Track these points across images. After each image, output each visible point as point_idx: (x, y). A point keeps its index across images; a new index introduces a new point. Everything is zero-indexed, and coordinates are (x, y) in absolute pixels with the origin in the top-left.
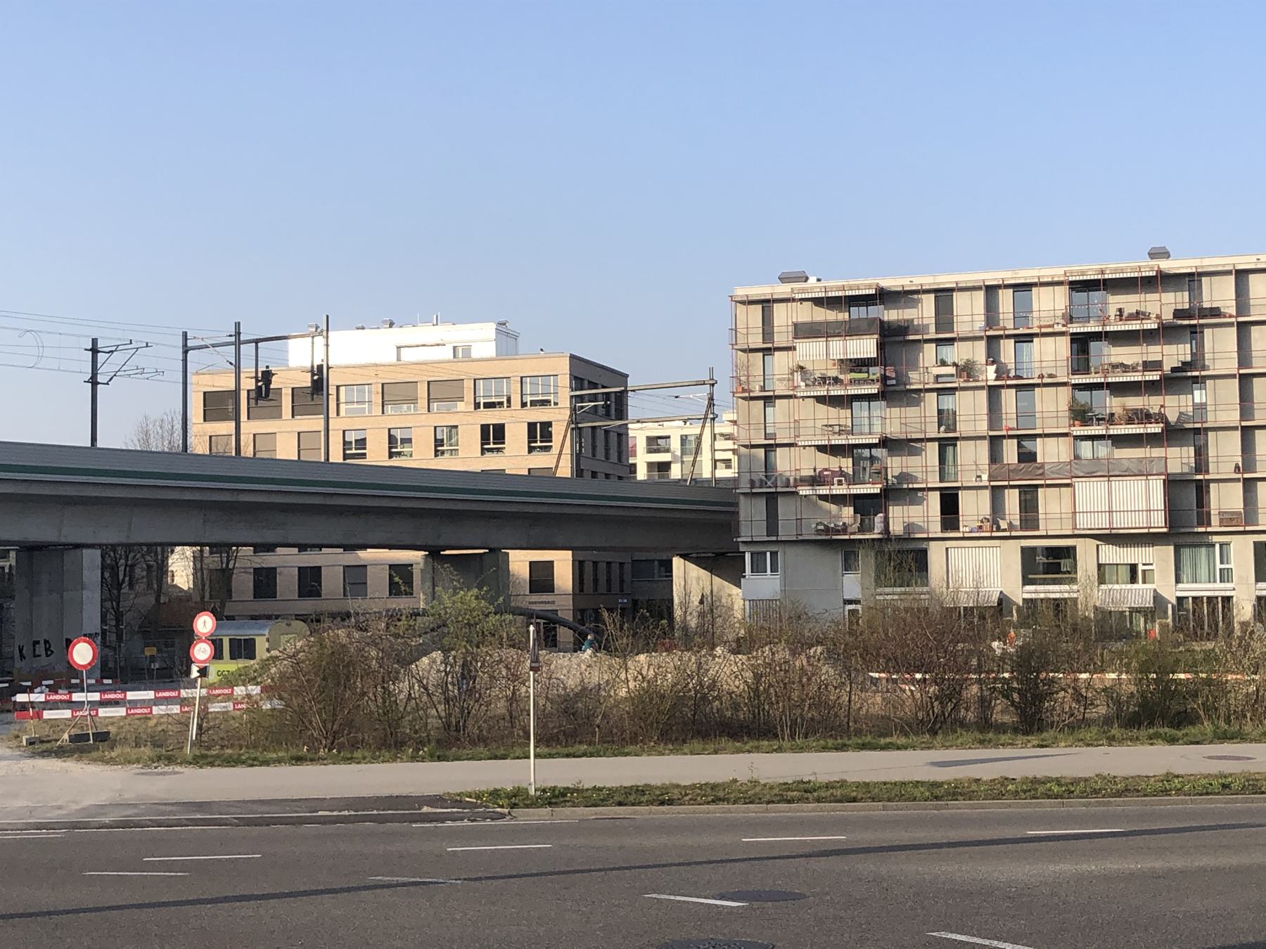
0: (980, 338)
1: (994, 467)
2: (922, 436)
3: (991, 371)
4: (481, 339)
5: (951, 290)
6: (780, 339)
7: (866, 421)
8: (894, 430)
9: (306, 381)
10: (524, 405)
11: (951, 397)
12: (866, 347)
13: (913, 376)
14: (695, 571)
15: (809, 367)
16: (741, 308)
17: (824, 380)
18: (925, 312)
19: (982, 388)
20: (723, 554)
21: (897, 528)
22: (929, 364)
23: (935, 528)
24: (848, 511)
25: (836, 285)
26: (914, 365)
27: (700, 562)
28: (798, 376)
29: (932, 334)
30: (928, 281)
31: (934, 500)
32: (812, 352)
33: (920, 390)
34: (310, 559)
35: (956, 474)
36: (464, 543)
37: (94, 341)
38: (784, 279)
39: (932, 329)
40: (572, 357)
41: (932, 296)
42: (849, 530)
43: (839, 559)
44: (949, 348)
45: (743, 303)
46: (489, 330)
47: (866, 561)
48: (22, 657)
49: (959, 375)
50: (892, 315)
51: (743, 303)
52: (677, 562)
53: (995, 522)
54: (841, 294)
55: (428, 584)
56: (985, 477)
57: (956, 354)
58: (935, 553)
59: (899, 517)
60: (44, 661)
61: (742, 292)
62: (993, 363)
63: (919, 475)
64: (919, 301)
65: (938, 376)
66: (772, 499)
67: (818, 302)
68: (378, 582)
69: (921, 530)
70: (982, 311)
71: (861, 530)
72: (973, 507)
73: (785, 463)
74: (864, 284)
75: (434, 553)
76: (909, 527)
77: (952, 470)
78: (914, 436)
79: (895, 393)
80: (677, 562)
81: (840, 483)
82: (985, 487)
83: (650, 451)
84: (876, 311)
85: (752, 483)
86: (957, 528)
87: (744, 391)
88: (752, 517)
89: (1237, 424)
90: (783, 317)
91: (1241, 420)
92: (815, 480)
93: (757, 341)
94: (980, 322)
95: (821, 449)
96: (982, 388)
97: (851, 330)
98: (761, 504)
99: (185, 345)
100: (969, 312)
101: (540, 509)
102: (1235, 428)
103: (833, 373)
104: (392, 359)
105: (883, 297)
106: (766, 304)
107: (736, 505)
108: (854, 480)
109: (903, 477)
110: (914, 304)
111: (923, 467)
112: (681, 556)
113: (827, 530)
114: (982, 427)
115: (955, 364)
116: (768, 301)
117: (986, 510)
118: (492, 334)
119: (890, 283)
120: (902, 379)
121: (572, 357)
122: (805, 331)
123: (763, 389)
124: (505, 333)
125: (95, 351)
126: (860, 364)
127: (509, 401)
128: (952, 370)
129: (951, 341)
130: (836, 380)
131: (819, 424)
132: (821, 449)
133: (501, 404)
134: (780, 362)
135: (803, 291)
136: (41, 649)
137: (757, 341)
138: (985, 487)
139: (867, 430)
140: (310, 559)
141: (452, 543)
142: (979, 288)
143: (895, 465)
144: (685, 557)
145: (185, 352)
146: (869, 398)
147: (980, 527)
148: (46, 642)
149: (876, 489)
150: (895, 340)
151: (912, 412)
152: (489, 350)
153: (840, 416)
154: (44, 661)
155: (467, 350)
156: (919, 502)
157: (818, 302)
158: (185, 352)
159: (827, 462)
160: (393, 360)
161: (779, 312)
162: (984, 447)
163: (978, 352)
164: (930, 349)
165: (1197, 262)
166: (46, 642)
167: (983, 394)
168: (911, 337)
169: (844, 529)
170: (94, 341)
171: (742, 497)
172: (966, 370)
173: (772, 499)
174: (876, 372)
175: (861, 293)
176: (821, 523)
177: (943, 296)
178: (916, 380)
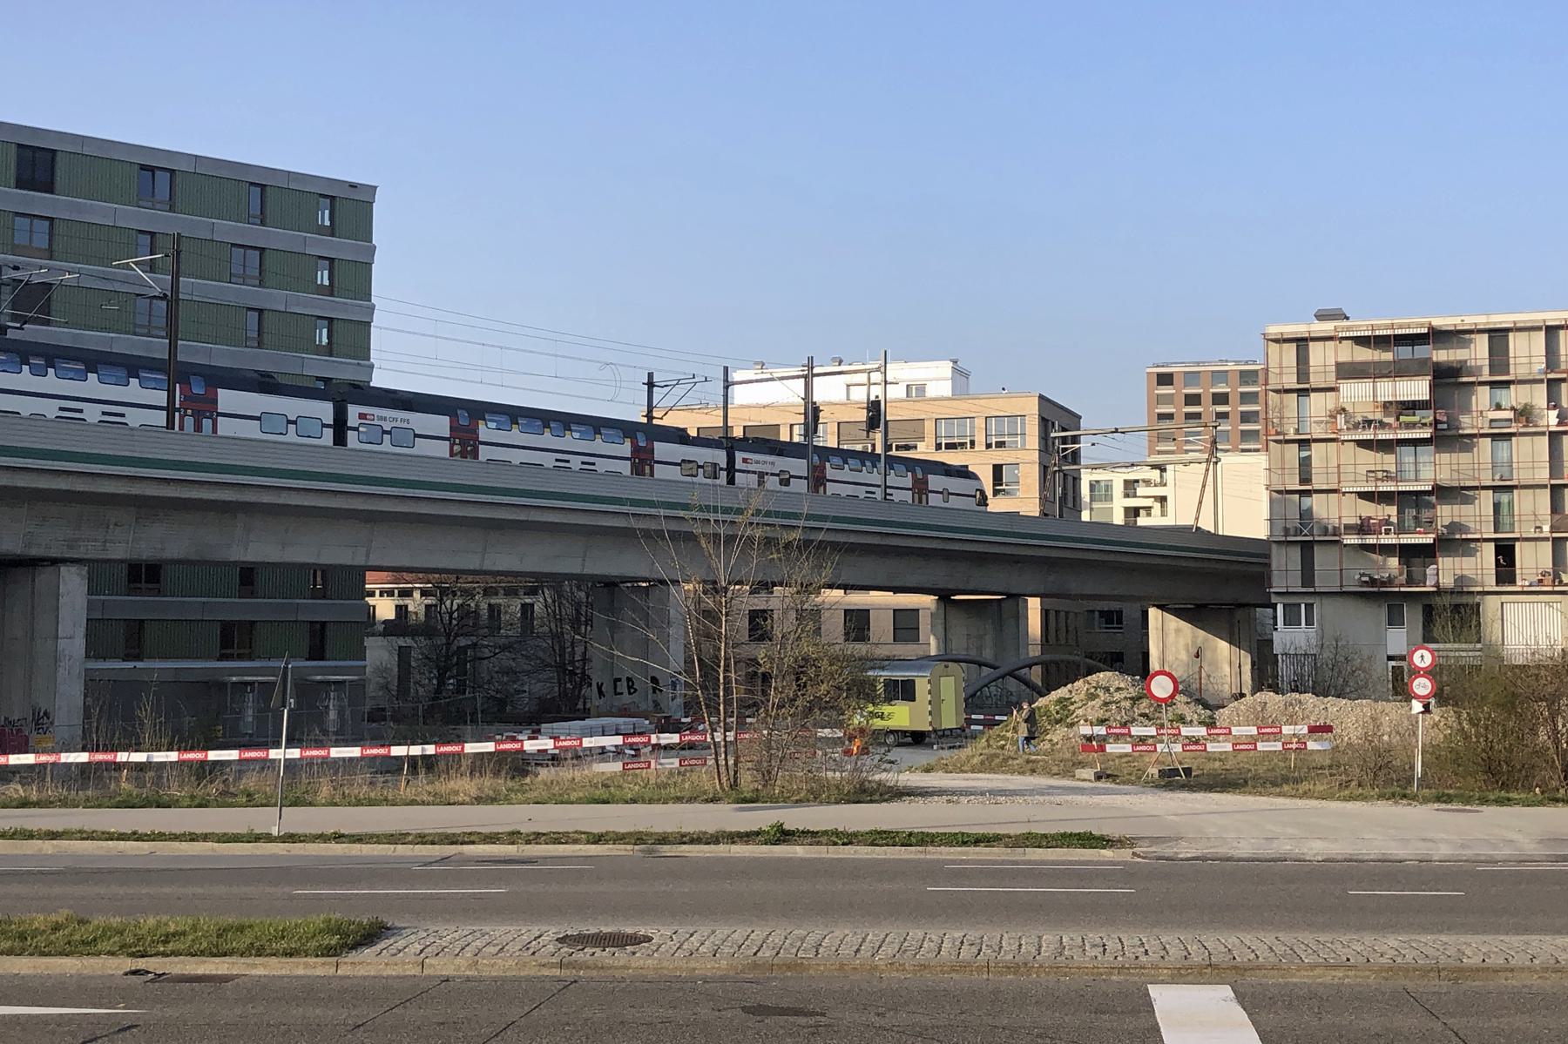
0: (1541, 381)
1: (1557, 517)
2: (1476, 483)
3: (1553, 416)
4: (937, 378)
5: (1507, 330)
6: (1315, 380)
7: (1412, 468)
8: (1445, 477)
9: (862, 416)
10: (989, 446)
11: (1505, 444)
12: (1418, 388)
13: (1465, 420)
14: (1173, 622)
15: (1349, 409)
16: (1274, 347)
17: (1368, 423)
18: (1478, 352)
19: (1543, 434)
20: (1205, 606)
21: (1447, 581)
22: (1481, 409)
23: (1490, 583)
24: (1394, 562)
25: (1383, 324)
26: (1467, 409)
27: (1179, 613)
28: (1341, 419)
29: (1486, 377)
30: (1482, 320)
31: (1489, 549)
32: (1357, 394)
33: (1474, 436)
34: (858, 599)
35: (1512, 525)
36: (993, 589)
37: (650, 375)
38: (1322, 316)
39: (1486, 370)
40: (1041, 397)
41: (1294, 345)
42: (1397, 582)
43: (1383, 613)
44: (1504, 392)
45: (1276, 341)
46: (946, 368)
47: (1413, 615)
48: (601, 693)
49: (1516, 420)
50: (1441, 356)
51: (1276, 341)
52: (1154, 614)
53: (1556, 576)
54: (1389, 332)
55: (940, 628)
56: (1546, 528)
57: (1515, 397)
58: (1491, 605)
59: (1445, 571)
60: (626, 698)
61: (1274, 330)
62: (1555, 407)
63: (1472, 525)
64: (1470, 341)
65: (1492, 421)
66: (1307, 548)
67: (1361, 341)
68: (834, 627)
69: (1474, 583)
70: (1487, 355)
71: (1410, 582)
72: (1532, 560)
73: (1325, 509)
74: (1415, 323)
75: (944, 597)
76: (1461, 579)
77: (1507, 520)
78: (1468, 484)
79: (1447, 438)
80: (1154, 614)
81: (1387, 532)
82: (1546, 539)
83: (1127, 496)
84: (1421, 351)
85: (1286, 530)
86: (1513, 582)
87: (1278, 433)
88: (1285, 571)
89: (1546, 482)
90: (1319, 356)
91: (1551, 477)
92: (1363, 528)
93: (1291, 381)
94: (1540, 364)
95: (1364, 496)
96: (1543, 434)
97: (1399, 371)
98: (1296, 554)
99: (726, 380)
100: (1527, 353)
101: (1054, 554)
102: (1545, 486)
103: (1378, 416)
104: (842, 397)
105: (1437, 336)
106: (1302, 342)
107: (1268, 556)
108: (1401, 529)
109: (1454, 527)
110: (1466, 344)
111: (1477, 516)
112: (1158, 607)
113: (1373, 582)
114: (1543, 475)
115: (1512, 408)
116: (1305, 339)
117: (1547, 564)
118: (949, 374)
119: (1440, 322)
120: (1453, 424)
121: (1041, 397)
122: (1348, 371)
123: (1297, 432)
124: (959, 373)
125: (651, 384)
126: (1412, 406)
127: (972, 443)
128: (1510, 415)
129: (1507, 384)
130: (1382, 425)
131: (1362, 470)
132: (1364, 496)
133: (963, 445)
134: (1318, 405)
135: (1349, 329)
136: (623, 687)
137: (1291, 381)
138: (1546, 539)
139: (1413, 476)
140: (858, 599)
141: (961, 587)
142: (1539, 329)
143: (1446, 513)
144: (1161, 607)
145: (726, 388)
146: (1415, 443)
147: (1540, 581)
148: (629, 679)
149: (1428, 539)
150: (1447, 379)
151: (1464, 457)
152: (946, 389)
153: (1388, 461)
154: (626, 698)
155: (921, 389)
156: (1471, 553)
157: (1361, 341)
158: (726, 388)
159: (1369, 509)
160: (843, 398)
161: (1316, 352)
162: (1545, 496)
163: (1539, 396)
164: (1484, 391)
165: (1457, 320)
166: (629, 679)
167: (1544, 441)
168: (1464, 379)
169: (1390, 582)
170: (650, 375)
171: (1274, 546)
172: (1524, 414)
173: (1307, 548)
174: (1428, 415)
175: (1411, 331)
176: (1362, 575)
177: (1498, 336)
178: (1468, 424)
